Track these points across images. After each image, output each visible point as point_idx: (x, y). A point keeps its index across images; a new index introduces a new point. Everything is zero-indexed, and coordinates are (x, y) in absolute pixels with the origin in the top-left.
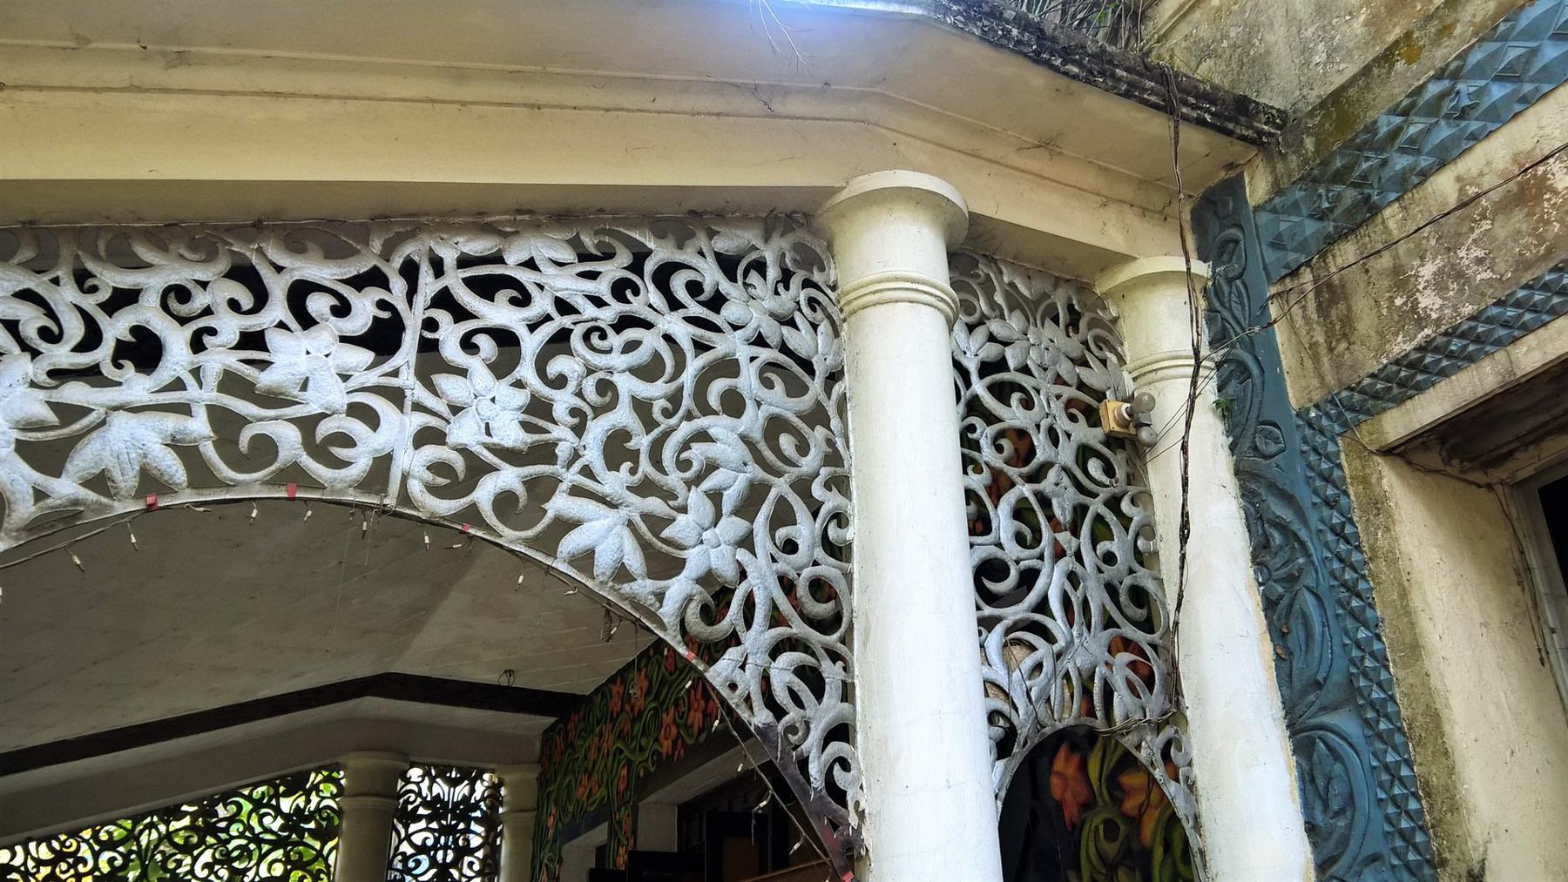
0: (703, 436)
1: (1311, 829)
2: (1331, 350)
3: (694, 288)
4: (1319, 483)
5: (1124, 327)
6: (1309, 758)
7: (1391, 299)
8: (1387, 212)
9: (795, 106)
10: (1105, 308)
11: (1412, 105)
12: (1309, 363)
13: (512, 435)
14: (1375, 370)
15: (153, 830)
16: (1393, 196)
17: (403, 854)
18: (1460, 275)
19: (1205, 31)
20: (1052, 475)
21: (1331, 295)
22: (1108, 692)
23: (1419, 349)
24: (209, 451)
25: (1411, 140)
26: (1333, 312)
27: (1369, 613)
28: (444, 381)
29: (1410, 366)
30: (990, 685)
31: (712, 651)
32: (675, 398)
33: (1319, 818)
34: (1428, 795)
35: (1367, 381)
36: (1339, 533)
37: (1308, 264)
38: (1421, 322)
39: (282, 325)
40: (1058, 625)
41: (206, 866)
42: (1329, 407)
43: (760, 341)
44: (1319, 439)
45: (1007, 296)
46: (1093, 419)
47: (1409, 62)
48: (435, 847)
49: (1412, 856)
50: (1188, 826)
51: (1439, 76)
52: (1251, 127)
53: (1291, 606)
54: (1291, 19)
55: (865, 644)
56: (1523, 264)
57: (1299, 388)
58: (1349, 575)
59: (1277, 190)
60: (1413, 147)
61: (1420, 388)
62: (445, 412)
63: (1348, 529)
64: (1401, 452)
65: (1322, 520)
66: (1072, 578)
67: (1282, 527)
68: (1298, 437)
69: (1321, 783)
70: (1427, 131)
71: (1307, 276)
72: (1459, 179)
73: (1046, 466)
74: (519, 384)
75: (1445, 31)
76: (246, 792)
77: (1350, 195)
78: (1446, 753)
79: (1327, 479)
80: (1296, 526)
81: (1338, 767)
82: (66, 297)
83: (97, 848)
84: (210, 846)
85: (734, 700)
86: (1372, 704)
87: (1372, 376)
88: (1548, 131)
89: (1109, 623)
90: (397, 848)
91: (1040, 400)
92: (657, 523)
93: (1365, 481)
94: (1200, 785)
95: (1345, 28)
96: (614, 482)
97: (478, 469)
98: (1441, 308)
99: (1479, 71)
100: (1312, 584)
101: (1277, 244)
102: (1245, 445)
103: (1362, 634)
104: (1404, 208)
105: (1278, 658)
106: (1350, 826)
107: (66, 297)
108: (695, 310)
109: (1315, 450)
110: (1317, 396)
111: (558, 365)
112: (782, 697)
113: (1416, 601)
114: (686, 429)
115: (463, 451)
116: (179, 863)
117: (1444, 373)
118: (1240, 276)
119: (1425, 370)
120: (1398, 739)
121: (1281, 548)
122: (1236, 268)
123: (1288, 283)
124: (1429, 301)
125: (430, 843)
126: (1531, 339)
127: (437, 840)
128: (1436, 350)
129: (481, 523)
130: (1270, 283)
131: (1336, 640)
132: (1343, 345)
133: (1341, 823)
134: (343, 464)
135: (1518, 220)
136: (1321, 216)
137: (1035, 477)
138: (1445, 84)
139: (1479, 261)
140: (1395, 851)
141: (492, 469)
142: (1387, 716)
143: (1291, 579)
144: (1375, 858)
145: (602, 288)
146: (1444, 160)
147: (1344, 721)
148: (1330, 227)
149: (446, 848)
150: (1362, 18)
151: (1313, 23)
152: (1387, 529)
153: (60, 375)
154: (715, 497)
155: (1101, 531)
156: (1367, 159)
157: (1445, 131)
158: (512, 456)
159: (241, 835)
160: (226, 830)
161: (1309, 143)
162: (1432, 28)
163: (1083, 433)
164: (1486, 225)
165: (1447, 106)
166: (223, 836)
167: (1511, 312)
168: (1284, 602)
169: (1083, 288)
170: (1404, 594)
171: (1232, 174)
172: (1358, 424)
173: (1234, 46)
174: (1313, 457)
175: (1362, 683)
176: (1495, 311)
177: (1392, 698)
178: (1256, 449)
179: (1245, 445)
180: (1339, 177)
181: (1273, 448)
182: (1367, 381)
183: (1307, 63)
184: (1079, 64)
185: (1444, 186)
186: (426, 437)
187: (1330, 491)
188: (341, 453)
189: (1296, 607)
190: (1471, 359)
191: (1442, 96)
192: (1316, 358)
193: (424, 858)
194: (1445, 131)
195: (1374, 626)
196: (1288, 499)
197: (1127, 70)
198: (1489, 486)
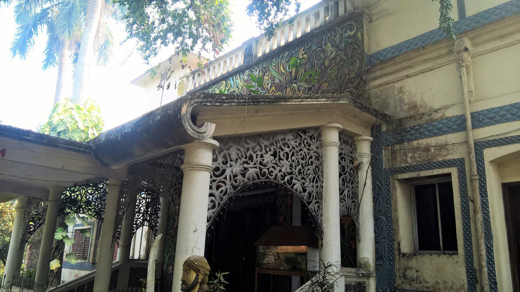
0: (309, 169)
1: (375, 232)
2: (392, 161)
3: (307, 143)
4: (386, 181)
5: (358, 146)
6: (376, 222)
7: (403, 157)
8: (405, 143)
9: (322, 110)
10: (355, 142)
11: (413, 128)
12: (388, 161)
13: (289, 171)
14: (398, 167)
15: (84, 190)
16: (407, 141)
17: (140, 199)
18: (415, 158)
19: (378, 92)
20: (347, 173)
21: (393, 152)
22: (351, 209)
23: (406, 166)
24: (259, 173)
25: (412, 134)
26: (393, 155)
27: (390, 203)
28: (281, 161)
29: (404, 169)
30: (211, 195)
31: (309, 203)
32: (306, 163)
33: (376, 231)
34: (394, 231)
35: (397, 168)
36: (388, 190)
37: (391, 145)
38: (407, 162)
39: (265, 153)
40: (346, 199)
41: (95, 199)
42: (390, 170)
43: (315, 152)
44: (387, 175)
45: (343, 141)
46: (353, 164)
47: (414, 120)
48: (146, 198)
49: (390, 239)
50: (358, 230)
51: (418, 125)
52: (386, 119)
53: (377, 199)
54: (395, 99)
55: (325, 202)
56: (424, 160)
57: (385, 165)
58: (388, 197)
59: (387, 130)
60: (412, 135)
61: (405, 173)
62: (282, 166)
63: (389, 190)
64: (400, 181)
65: (385, 187)
66: (349, 191)
67: (379, 186)
68: (384, 173)
69: (378, 226)
70: (415, 133)
71: (390, 148)
72: (418, 143)
73: (347, 172)
74: (289, 162)
75: (421, 118)
76: (105, 181)
77: (400, 138)
78: (398, 226)
79: (387, 181)
80: (381, 187)
81: (381, 224)
82: (242, 149)
83: (71, 193)
84: (96, 194)
85: (311, 211)
86: (388, 217)
87: (398, 168)
88: (432, 142)
89: (352, 198)
90: (138, 198)
91: (346, 160)
92: (304, 184)
93: (393, 183)
94: (360, 223)
95: (404, 106)
96: (299, 177)
97: (285, 176)
98: (410, 162)
99: (425, 128)
100: (382, 196)
101: (386, 140)
102: (374, 171)
103: (389, 206)
104: (408, 144)
105: (374, 206)
106: (382, 232)
107: (242, 149)
108: (308, 147)
109: (386, 176)
110: (388, 167)
111: (293, 158)
112: (316, 210)
113: (398, 203)
114: (307, 168)
115: (284, 173)
116: (89, 197)
117: (409, 172)
118: (378, 142)
119: (406, 170)
120: (391, 222)
121: (378, 189)
122: (378, 141)
123: (387, 147)
124: (409, 160)
125: (145, 197)
126: (423, 172)
127: (147, 197)
128: (409, 168)
129: (286, 185)
130: (384, 146)
131: (384, 206)
132: (394, 161)
133: (380, 232)
134: (272, 176)
135: (425, 153)
136: (395, 139)
137: (345, 174)
138: (419, 127)
139: (418, 157)
140: (388, 237)
141: (287, 176)
142: (390, 219)
143: (378, 195)
144: (384, 238)
145: (297, 144)
146: (416, 139)
147: (383, 218)
148: (396, 141)
149: (149, 198)
150: (407, 107)
151: (398, 103)
152: (395, 192)
153: (244, 163)
154: (310, 179)
155: (352, 183)
156: (404, 133)
157: (417, 135)
158: (289, 174)
159: (103, 192)
160: (100, 190)
161: (395, 125)
162: (419, 117)
163: (351, 166)
164: (420, 152)
165: (418, 131)
166: (100, 192)
167: (421, 167)
168: (376, 198)
169: (353, 138)
170: (396, 202)
171: (380, 124)
172: (394, 174)
173: (383, 99)
174: (386, 177)
175: (387, 213)
176: (419, 166)
177: (392, 216)
178: (376, 172)
179: (374, 171)
180: (399, 134)
181: (379, 173)
182: (397, 168)
183: (396, 109)
184: (366, 110)
185: (415, 143)
186: (280, 171)
187: (388, 183)
188: (272, 174)
189: (378, 199)
190: (414, 171)
191: (418, 129)
192: (389, 161)
193: (144, 200)
194: (417, 135)
195: (391, 205)
196: (380, 182)
197: (371, 110)
198: (408, 184)
